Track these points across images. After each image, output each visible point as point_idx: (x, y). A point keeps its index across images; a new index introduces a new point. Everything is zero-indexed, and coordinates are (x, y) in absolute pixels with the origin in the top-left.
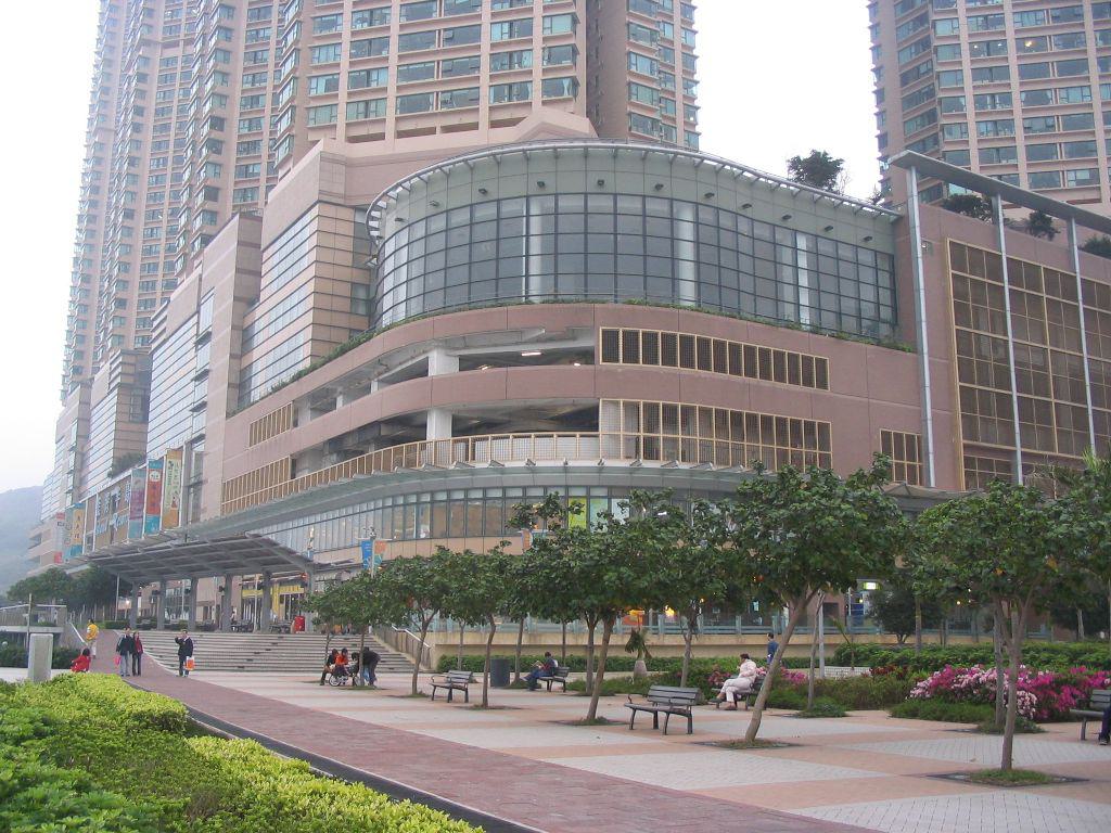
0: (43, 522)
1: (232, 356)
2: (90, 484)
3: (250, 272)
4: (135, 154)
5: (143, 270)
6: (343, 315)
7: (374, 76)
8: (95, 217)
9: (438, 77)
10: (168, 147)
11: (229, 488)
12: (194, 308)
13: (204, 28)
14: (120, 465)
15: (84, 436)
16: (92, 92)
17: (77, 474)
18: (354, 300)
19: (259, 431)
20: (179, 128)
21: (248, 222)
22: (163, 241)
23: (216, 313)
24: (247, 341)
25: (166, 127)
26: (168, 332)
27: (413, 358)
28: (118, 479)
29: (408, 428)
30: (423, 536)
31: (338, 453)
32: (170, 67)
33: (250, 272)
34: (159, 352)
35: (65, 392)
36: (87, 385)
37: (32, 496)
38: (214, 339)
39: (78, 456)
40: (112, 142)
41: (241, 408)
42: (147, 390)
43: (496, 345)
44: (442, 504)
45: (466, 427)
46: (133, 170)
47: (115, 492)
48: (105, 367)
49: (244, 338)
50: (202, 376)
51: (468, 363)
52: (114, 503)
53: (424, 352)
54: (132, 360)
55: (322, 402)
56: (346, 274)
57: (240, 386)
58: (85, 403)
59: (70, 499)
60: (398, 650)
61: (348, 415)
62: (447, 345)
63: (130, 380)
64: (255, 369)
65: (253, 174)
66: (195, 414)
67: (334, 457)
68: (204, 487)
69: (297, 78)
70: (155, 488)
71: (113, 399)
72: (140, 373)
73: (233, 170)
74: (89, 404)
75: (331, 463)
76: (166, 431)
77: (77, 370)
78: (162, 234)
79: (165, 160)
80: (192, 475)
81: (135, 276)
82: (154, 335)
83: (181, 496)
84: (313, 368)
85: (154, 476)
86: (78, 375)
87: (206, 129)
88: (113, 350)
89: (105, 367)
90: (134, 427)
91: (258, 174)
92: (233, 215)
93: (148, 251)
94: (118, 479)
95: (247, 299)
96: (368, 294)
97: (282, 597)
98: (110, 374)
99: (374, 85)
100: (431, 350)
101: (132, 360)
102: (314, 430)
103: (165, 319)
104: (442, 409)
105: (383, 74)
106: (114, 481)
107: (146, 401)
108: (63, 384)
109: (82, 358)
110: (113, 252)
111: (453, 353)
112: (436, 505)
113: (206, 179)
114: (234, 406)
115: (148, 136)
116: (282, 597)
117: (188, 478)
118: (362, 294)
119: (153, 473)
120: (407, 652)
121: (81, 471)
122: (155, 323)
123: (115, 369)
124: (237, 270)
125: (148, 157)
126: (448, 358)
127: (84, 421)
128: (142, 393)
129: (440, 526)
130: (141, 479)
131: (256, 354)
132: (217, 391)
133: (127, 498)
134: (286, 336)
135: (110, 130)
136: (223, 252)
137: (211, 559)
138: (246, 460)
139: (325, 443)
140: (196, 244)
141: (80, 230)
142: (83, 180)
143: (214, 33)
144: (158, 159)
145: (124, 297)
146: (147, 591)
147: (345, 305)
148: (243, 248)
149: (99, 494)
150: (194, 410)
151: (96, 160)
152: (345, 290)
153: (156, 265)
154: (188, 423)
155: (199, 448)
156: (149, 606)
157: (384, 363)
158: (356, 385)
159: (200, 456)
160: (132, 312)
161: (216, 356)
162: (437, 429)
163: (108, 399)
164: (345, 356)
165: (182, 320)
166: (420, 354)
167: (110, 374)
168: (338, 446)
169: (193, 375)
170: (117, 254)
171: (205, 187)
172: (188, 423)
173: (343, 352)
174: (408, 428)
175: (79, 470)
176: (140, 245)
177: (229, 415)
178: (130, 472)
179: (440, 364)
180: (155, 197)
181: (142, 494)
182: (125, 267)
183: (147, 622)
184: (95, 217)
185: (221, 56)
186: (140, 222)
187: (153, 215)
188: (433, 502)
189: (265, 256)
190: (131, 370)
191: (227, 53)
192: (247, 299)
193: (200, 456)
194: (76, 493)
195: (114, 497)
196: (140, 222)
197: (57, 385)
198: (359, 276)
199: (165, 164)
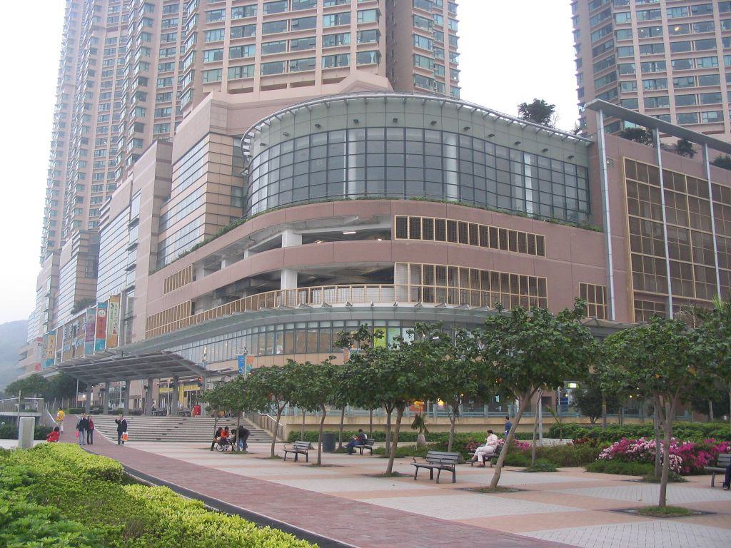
0: (28, 344)
1: (153, 234)
2: (59, 319)
3: (165, 179)
4: (89, 101)
5: (94, 177)
6: (226, 207)
7: (246, 50)
8: (62, 143)
9: (288, 51)
10: (110, 97)
11: (151, 321)
12: (128, 203)
13: (134, 18)
14: (79, 306)
15: (55, 287)
16: (61, 61)
17: (51, 312)
18: (233, 197)
19: (171, 284)
20: (118, 84)
21: (163, 146)
22: (107, 158)
23: (142, 206)
24: (162, 224)
25: (109, 84)
26: (111, 218)
27: (272, 235)
28: (77, 315)
29: (268, 281)
30: (278, 352)
31: (223, 298)
32: (112, 44)
33: (165, 179)
34: (105, 232)
35: (42, 258)
36: (57, 253)
37: (21, 326)
38: (141, 223)
39: (51, 300)
40: (73, 94)
41: (158, 269)
42: (97, 257)
43: (326, 227)
44: (291, 332)
45: (307, 281)
46: (87, 112)
47: (76, 323)
48: (69, 242)
49: (160, 222)
50: (133, 247)
51: (308, 239)
52: (75, 331)
53: (279, 232)
54: (87, 237)
55: (212, 264)
56: (228, 180)
57: (158, 254)
58: (56, 265)
59: (46, 328)
60: (262, 428)
61: (229, 273)
62: (294, 227)
63: (86, 250)
64: (168, 243)
65: (167, 115)
66: (128, 272)
67: (220, 301)
68: (134, 320)
69: (195, 51)
70: (102, 321)
71: (74, 262)
72: (92, 246)
73: (153, 112)
74: (58, 266)
75: (218, 305)
76: (109, 283)
77: (51, 244)
78: (107, 154)
79: (109, 105)
80: (126, 313)
81: (89, 182)
82: (102, 220)
83: (119, 326)
84: (206, 242)
85: (102, 313)
86: (52, 247)
87: (136, 85)
88: (74, 230)
89: (69, 242)
90: (88, 281)
91: (170, 115)
92: (154, 142)
93: (97, 165)
94: (77, 315)
95: (163, 197)
96: (242, 194)
97: (185, 392)
98: (73, 246)
99: (246, 56)
100: (283, 230)
101: (87, 237)
102: (207, 283)
103: (109, 210)
104: (291, 269)
105: (252, 49)
106: (75, 317)
107: (96, 264)
108: (42, 252)
109: (54, 235)
110: (74, 166)
111: (298, 232)
112: (287, 332)
113: (136, 118)
114: (154, 267)
115: (97, 90)
116: (185, 392)
117: (124, 314)
118: (238, 193)
119: (101, 311)
120: (268, 429)
121: (53, 310)
122: (102, 213)
123: (76, 243)
124: (156, 178)
125: (97, 103)
126: (295, 235)
127: (55, 277)
128: (93, 258)
129: (290, 346)
130: (93, 315)
131: (168, 233)
132: (142, 257)
133: (84, 328)
134: (188, 221)
135: (73, 86)
136: (147, 166)
137: (139, 368)
138: (162, 303)
139: (214, 291)
140: (129, 160)
141: (52, 152)
142: (55, 118)
143: (141, 22)
144: (104, 105)
145: (82, 196)
146: (97, 389)
147: (227, 201)
148: (160, 163)
149: (65, 325)
150: (127, 270)
151: (63, 105)
152: (227, 191)
153: (103, 175)
154: (124, 278)
155: (131, 295)
156: (98, 399)
157: (253, 239)
158: (234, 253)
159: (131, 300)
160: (87, 205)
161: (142, 234)
162: (288, 282)
163: (71, 262)
164: (227, 234)
165: (120, 211)
166: (276, 233)
167: (73, 246)
168: (222, 293)
169: (127, 246)
170: (77, 167)
171: (135, 123)
172: (124, 278)
173: (226, 231)
174: (268, 281)
175: (52, 309)
176: (92, 161)
177: (150, 273)
178: (85, 310)
179: (289, 239)
180: (102, 130)
181: (93, 325)
182: (82, 175)
183: (97, 409)
184: (62, 143)
185: (145, 37)
186: (92, 146)
187: (100, 141)
188: (285, 330)
189: (175, 168)
190: (86, 243)
191: (149, 35)
192: (163, 197)
193: (131, 300)
194: (50, 324)
195: (75, 327)
196: (92, 146)
197: (37, 253)
198: (236, 182)
199: (108, 108)
